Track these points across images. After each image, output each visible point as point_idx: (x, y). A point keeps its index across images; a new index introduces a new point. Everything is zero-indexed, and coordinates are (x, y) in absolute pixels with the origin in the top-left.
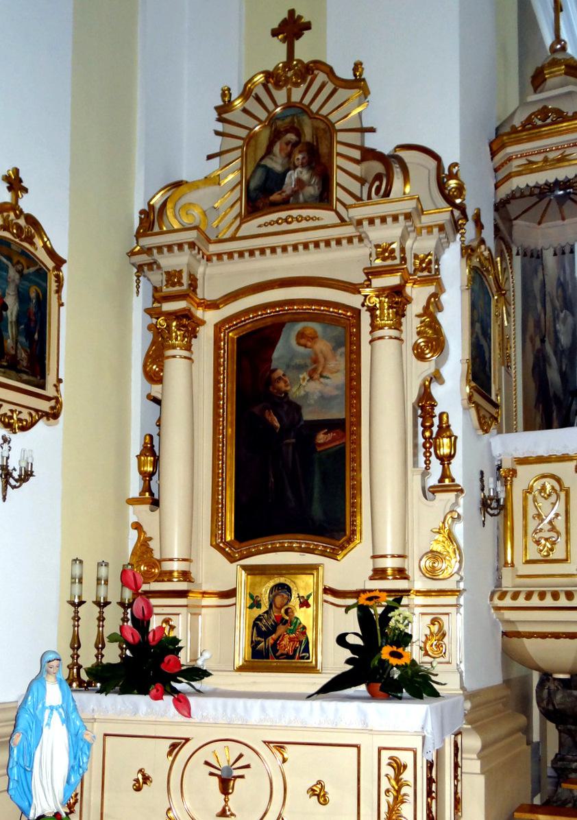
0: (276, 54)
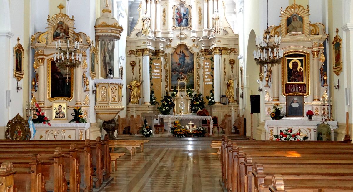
0: (58, 11)
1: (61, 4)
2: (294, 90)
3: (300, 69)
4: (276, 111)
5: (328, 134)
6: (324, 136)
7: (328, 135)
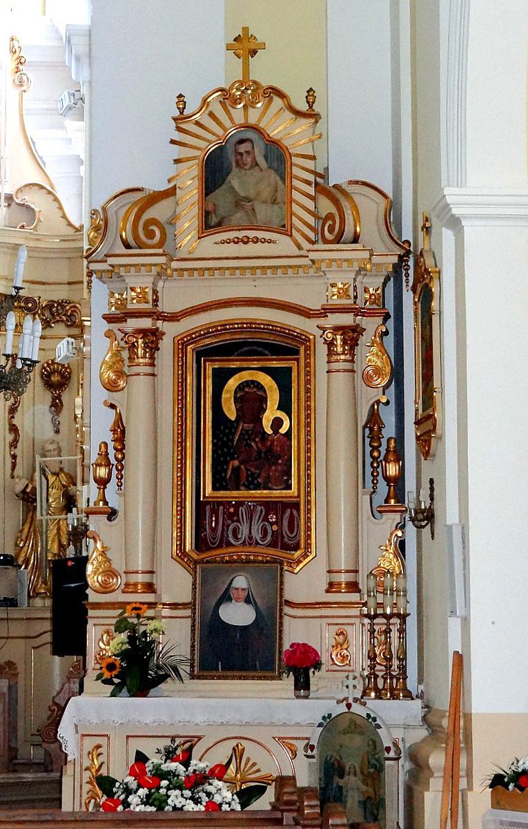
1: (245, 30)
2: (244, 530)
3: (277, 423)
4: (127, 646)
5: (372, 770)
6: (352, 778)
7: (370, 775)
